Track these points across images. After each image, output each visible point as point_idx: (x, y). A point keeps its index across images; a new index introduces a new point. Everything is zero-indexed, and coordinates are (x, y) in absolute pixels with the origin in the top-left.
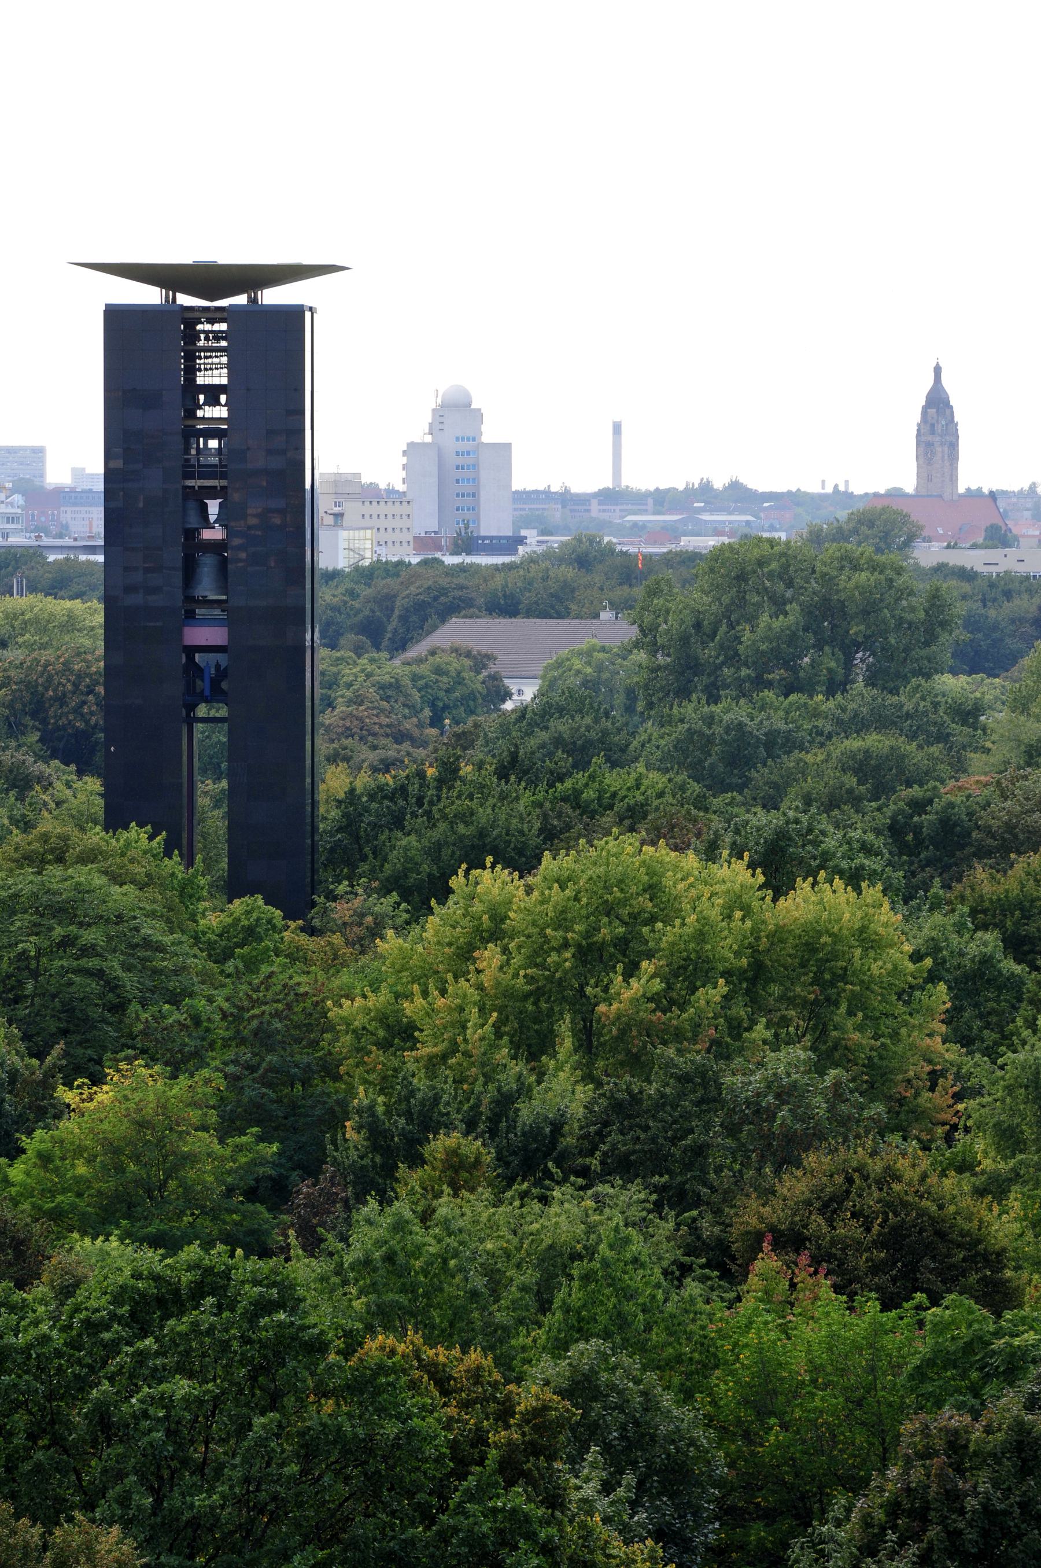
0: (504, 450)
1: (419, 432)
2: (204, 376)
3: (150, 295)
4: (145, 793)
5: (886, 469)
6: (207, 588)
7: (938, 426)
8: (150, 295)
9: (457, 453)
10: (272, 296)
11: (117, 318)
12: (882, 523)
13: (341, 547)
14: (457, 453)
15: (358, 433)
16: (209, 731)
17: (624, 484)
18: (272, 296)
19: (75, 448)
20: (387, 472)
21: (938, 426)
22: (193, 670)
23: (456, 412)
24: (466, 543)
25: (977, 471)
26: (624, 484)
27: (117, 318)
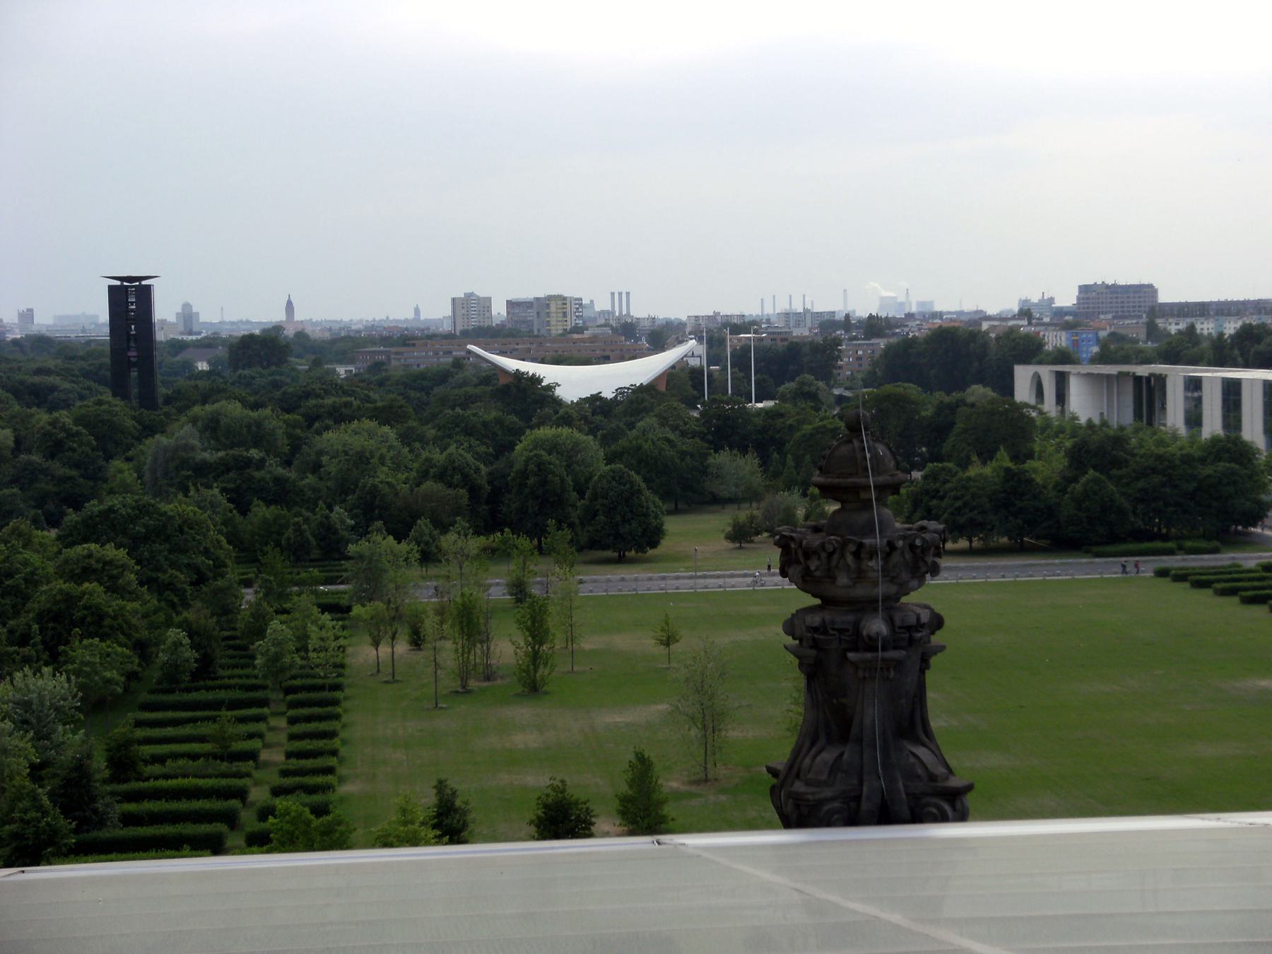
0: (1084, 289)
1: (180, 310)
2: (130, 299)
3: (118, 283)
4: (120, 389)
5: (411, 316)
6: (132, 344)
7: (290, 307)
8: (118, 283)
9: (188, 315)
10: (144, 283)
11: (111, 288)
12: (278, 328)
13: (160, 336)
14: (188, 315)
15: (165, 310)
16: (616, 554)
17: (422, 318)
18: (144, 283)
19: (103, 315)
20: (172, 318)
21: (290, 307)
22: (130, 362)
23: (187, 306)
24: (190, 333)
25: (299, 316)
26: (422, 318)
27: (111, 288)
